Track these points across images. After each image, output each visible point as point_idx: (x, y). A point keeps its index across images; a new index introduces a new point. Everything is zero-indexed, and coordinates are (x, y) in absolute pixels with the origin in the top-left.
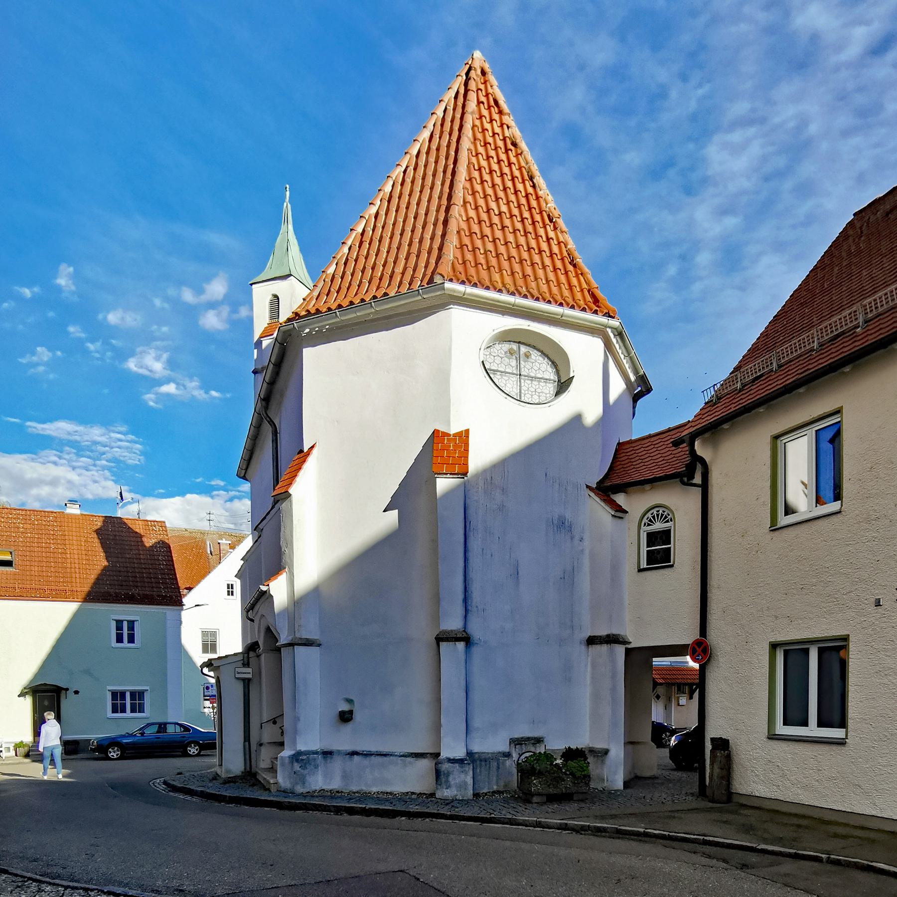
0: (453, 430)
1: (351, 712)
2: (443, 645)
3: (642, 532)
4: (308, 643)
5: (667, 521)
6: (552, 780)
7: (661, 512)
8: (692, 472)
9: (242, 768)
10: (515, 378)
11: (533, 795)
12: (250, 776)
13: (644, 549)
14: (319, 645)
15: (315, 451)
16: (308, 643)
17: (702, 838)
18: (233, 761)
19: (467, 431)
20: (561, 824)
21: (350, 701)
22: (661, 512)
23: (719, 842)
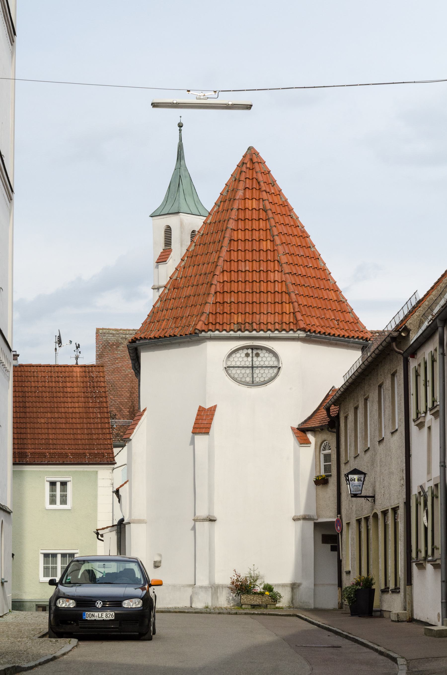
1: (160, 562)
2: (197, 524)
4: (140, 522)
14: (146, 523)
15: (146, 413)
16: (140, 522)
19: (215, 406)
21: (160, 555)
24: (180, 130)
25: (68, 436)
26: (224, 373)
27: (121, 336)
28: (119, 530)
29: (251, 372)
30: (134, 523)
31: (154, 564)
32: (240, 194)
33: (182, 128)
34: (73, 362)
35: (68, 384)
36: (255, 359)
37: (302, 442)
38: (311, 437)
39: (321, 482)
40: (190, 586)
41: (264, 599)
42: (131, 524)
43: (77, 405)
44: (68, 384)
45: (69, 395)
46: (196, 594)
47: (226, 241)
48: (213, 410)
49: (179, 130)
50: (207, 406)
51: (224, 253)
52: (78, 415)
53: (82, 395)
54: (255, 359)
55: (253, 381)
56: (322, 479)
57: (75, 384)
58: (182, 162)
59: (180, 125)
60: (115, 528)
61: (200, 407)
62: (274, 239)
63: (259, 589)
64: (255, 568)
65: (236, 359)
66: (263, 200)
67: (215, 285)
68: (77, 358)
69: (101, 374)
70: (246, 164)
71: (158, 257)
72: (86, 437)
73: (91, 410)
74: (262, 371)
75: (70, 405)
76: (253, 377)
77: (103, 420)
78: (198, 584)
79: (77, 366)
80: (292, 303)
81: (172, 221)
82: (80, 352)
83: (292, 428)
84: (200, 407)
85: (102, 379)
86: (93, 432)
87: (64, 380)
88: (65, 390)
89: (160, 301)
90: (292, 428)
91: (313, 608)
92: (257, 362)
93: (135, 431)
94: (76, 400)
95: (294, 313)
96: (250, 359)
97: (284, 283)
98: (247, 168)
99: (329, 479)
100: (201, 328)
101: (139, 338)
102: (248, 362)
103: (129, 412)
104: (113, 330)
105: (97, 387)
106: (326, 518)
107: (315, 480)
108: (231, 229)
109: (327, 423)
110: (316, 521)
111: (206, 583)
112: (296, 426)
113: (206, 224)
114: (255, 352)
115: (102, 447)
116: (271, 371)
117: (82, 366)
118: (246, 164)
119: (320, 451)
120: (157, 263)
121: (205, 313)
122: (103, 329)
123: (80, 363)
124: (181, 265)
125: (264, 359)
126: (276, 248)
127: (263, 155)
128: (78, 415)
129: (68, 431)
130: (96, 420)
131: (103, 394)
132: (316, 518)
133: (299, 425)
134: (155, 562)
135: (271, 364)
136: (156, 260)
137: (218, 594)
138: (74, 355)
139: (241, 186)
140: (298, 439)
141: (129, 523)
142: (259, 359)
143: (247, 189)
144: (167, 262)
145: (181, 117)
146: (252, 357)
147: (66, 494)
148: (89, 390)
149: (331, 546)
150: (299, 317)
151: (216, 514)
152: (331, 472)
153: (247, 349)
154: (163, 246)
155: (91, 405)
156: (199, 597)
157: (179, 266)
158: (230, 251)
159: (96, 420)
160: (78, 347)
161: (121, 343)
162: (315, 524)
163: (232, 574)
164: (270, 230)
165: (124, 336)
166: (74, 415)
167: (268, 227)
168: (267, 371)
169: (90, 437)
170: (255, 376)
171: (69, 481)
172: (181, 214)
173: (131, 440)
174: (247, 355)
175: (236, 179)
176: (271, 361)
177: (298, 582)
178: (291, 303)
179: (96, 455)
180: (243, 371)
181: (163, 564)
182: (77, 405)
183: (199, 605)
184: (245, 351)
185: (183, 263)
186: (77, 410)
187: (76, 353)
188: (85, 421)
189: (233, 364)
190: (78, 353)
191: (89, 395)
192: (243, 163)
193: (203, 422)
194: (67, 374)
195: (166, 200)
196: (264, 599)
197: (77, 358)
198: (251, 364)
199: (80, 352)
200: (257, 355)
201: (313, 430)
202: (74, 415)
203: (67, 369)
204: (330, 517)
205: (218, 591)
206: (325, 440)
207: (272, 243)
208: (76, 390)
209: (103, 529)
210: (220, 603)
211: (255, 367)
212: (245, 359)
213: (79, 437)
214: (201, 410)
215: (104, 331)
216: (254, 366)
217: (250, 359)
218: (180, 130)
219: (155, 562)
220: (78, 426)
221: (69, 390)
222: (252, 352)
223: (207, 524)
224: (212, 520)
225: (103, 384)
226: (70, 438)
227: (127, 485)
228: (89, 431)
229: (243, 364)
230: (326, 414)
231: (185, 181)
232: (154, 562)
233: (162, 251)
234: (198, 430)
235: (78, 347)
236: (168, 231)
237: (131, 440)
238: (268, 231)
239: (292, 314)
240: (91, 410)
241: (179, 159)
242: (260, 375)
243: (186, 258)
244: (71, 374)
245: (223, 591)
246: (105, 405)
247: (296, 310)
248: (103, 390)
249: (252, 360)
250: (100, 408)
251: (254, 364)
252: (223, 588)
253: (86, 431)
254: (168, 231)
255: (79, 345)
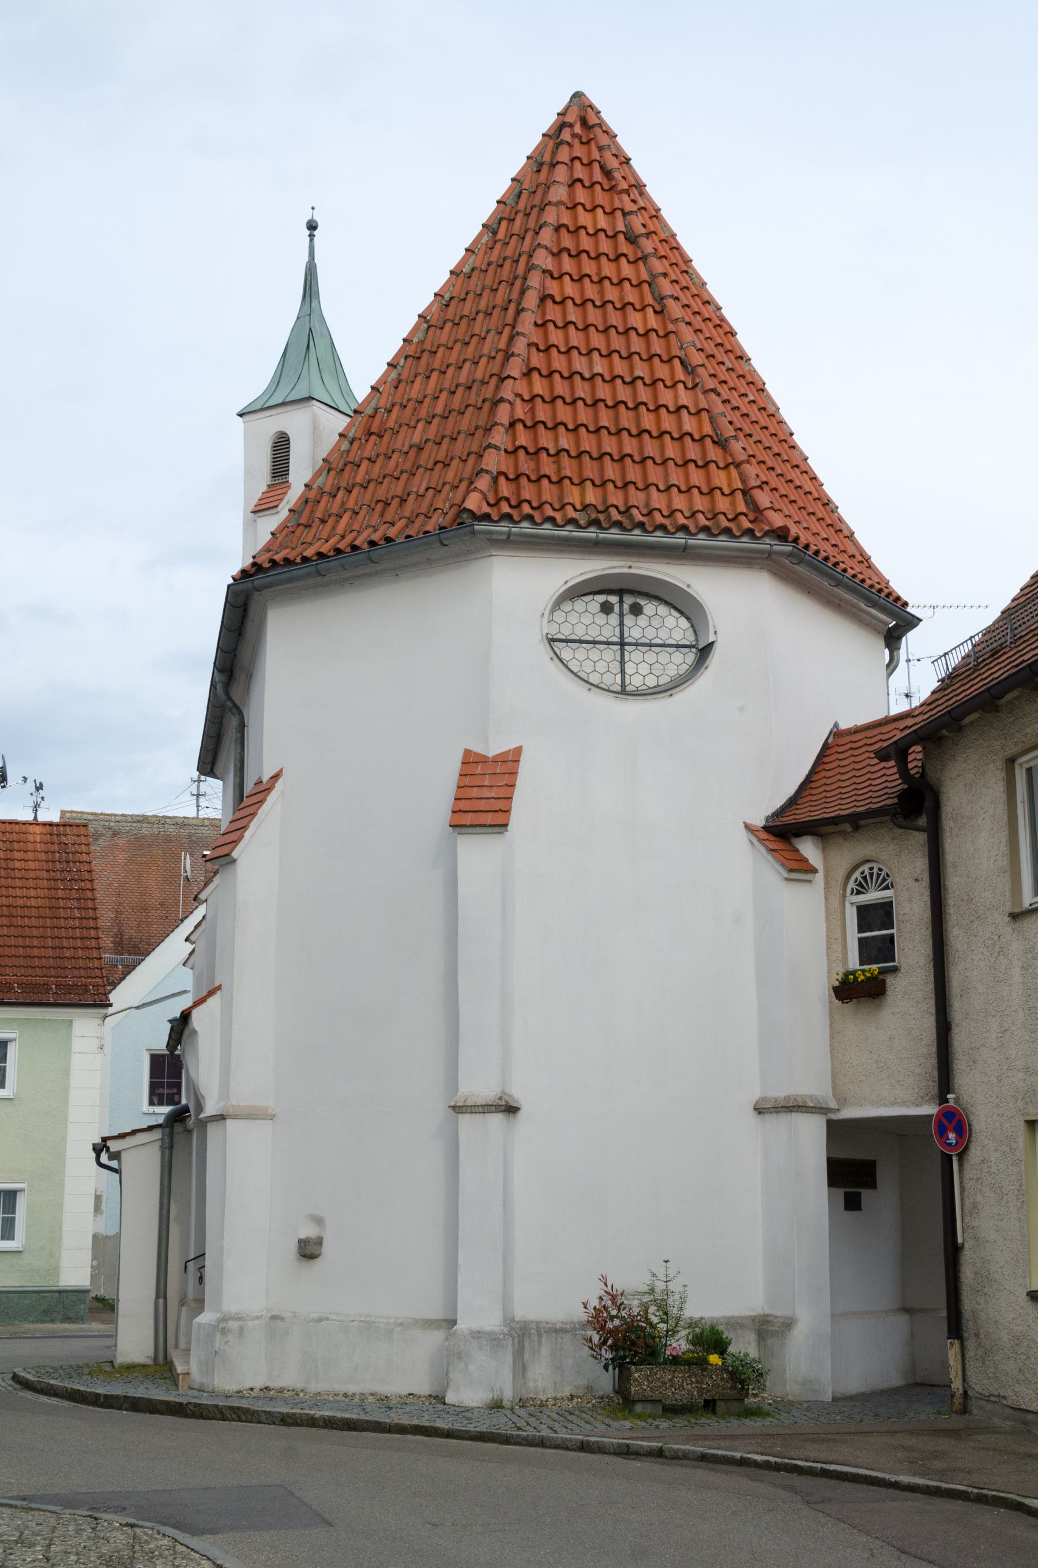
0: (492, 752)
1: (319, 1242)
2: (465, 1120)
3: (847, 905)
4: (253, 1115)
5: (887, 888)
6: (661, 1377)
7: (867, 872)
8: (917, 805)
9: (150, 1351)
10: (611, 654)
11: (634, 1402)
12: (162, 1367)
13: (853, 935)
14: (272, 1117)
15: (279, 785)
16: (253, 1115)
17: (819, 1465)
18: (133, 1340)
19: (518, 751)
20: (620, 1445)
21: (318, 1221)
22: (875, 870)
23: (841, 1473)
24: (312, 236)
25: (14, 951)
26: (543, 652)
27: (102, 823)
28: (167, 1141)
29: (618, 658)
30: (235, 1117)
31: (300, 1248)
32: (559, 193)
33: (315, 233)
34: (29, 817)
35: (17, 855)
36: (629, 620)
37: (793, 865)
38: (809, 849)
39: (857, 991)
40: (429, 1324)
41: (707, 1383)
42: (229, 1122)
43: (32, 893)
44: (17, 855)
45: (18, 874)
46: (460, 1358)
47: (531, 300)
48: (508, 763)
49: (310, 235)
50: (493, 748)
51: (527, 324)
52: (34, 912)
53: (45, 874)
54: (629, 620)
55: (623, 685)
56: (868, 979)
57: (31, 855)
58: (314, 304)
59: (312, 226)
60: (157, 1135)
61: (467, 752)
62: (664, 307)
63: (680, 1344)
64: (672, 1273)
65: (573, 618)
66: (625, 214)
67: (510, 403)
68: (36, 807)
69: (83, 839)
70: (571, 126)
71: (255, 501)
72: (50, 953)
73: (61, 903)
74: (651, 657)
75: (19, 892)
76: (623, 672)
77: (85, 923)
78: (464, 1324)
79: (35, 823)
80: (738, 465)
81: (294, 422)
82: (43, 798)
83: (747, 826)
84: (467, 752)
85: (84, 848)
86: (66, 944)
87: (9, 847)
88: (11, 865)
89: (325, 472)
90: (747, 826)
91: (828, 1397)
92: (636, 629)
93: (247, 834)
94: (31, 883)
95: (744, 492)
96: (614, 619)
97: (704, 414)
98: (574, 135)
99: (890, 980)
100: (480, 508)
101: (266, 565)
102: (607, 627)
103: (113, 942)
104: (88, 814)
105: (74, 862)
106: (879, 1104)
107: (837, 984)
108: (544, 272)
109: (896, 800)
110: (834, 1117)
111: (491, 1321)
112: (759, 822)
113: (458, 275)
114: (628, 600)
115: (82, 973)
116: (678, 657)
117: (44, 824)
118: (571, 126)
119: (844, 897)
120: (254, 512)
121: (487, 472)
122: (72, 812)
123: (41, 818)
124: (389, 379)
125: (656, 622)
126: (671, 327)
127: (611, 117)
128: (34, 912)
129: (12, 941)
130: (71, 923)
131: (87, 876)
132: (833, 1105)
133: (767, 819)
134: (303, 1243)
135: (678, 637)
136: (252, 507)
137: (527, 1355)
138: (30, 801)
139: (561, 174)
140: (775, 858)
141: (221, 1118)
142: (642, 621)
143: (578, 185)
144: (279, 508)
145: (313, 208)
146: (621, 615)
147: (5, 1067)
148: (58, 866)
149: (846, 1194)
150: (763, 499)
151: (519, 1094)
152: (894, 961)
153: (610, 592)
154: (269, 477)
155: (60, 893)
156: (471, 1367)
157: (383, 380)
158: (544, 324)
159: (71, 923)
160: (39, 788)
161: (102, 835)
162: (831, 1125)
163: (598, 1290)
164: (650, 284)
165: (107, 824)
166: (27, 912)
167: (645, 276)
168: (664, 656)
169: (57, 952)
170: (629, 668)
171: (11, 1040)
172: (314, 402)
173: (234, 861)
174: (606, 608)
175: (540, 163)
176: (673, 627)
177: (780, 1312)
178: (732, 467)
179: (70, 989)
180: (595, 654)
181: (327, 1248)
182: (32, 893)
183: (469, 1393)
184: (601, 598)
185: (394, 375)
186: (33, 902)
187: (34, 798)
188: (48, 922)
189: (566, 632)
190: (39, 800)
191: (58, 875)
192: (561, 125)
193: (484, 796)
194: (15, 837)
195: (278, 380)
196: (707, 1383)
197: (36, 807)
198: (618, 633)
199: (43, 798)
200: (636, 610)
201: (819, 829)
202: (27, 912)
203: (17, 828)
204: (903, 1103)
205: (526, 1344)
206: (868, 861)
207: (659, 317)
208: (31, 865)
209: (122, 1136)
210: (531, 1384)
211: (630, 644)
212: (601, 618)
213: (36, 952)
214: (471, 761)
215: (74, 815)
216: (626, 641)
217: (614, 619)
218: (312, 236)
219: (303, 1243)
220: (35, 932)
221: (18, 864)
222: (621, 602)
223: (497, 1120)
224: (511, 1110)
225: (85, 857)
226: (17, 954)
227: (213, 1002)
228: (57, 942)
229: (593, 633)
230: (895, 770)
231: (320, 342)
232: (300, 1241)
233: (265, 488)
234: (468, 819)
235: (39, 788)
236: (281, 446)
237: (234, 861)
238: (646, 286)
239: (739, 495)
240: (61, 903)
241: (308, 296)
242: (642, 669)
243: (402, 361)
244: (22, 837)
245: (540, 1343)
246: (89, 894)
247: (754, 482)
248: (86, 868)
249: (622, 624)
250: (79, 899)
251: (626, 635)
252: (540, 1335)
253: (50, 942)
254: (281, 446)
255: (41, 784)
